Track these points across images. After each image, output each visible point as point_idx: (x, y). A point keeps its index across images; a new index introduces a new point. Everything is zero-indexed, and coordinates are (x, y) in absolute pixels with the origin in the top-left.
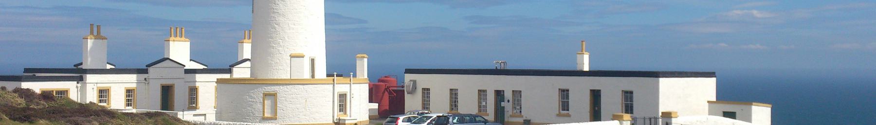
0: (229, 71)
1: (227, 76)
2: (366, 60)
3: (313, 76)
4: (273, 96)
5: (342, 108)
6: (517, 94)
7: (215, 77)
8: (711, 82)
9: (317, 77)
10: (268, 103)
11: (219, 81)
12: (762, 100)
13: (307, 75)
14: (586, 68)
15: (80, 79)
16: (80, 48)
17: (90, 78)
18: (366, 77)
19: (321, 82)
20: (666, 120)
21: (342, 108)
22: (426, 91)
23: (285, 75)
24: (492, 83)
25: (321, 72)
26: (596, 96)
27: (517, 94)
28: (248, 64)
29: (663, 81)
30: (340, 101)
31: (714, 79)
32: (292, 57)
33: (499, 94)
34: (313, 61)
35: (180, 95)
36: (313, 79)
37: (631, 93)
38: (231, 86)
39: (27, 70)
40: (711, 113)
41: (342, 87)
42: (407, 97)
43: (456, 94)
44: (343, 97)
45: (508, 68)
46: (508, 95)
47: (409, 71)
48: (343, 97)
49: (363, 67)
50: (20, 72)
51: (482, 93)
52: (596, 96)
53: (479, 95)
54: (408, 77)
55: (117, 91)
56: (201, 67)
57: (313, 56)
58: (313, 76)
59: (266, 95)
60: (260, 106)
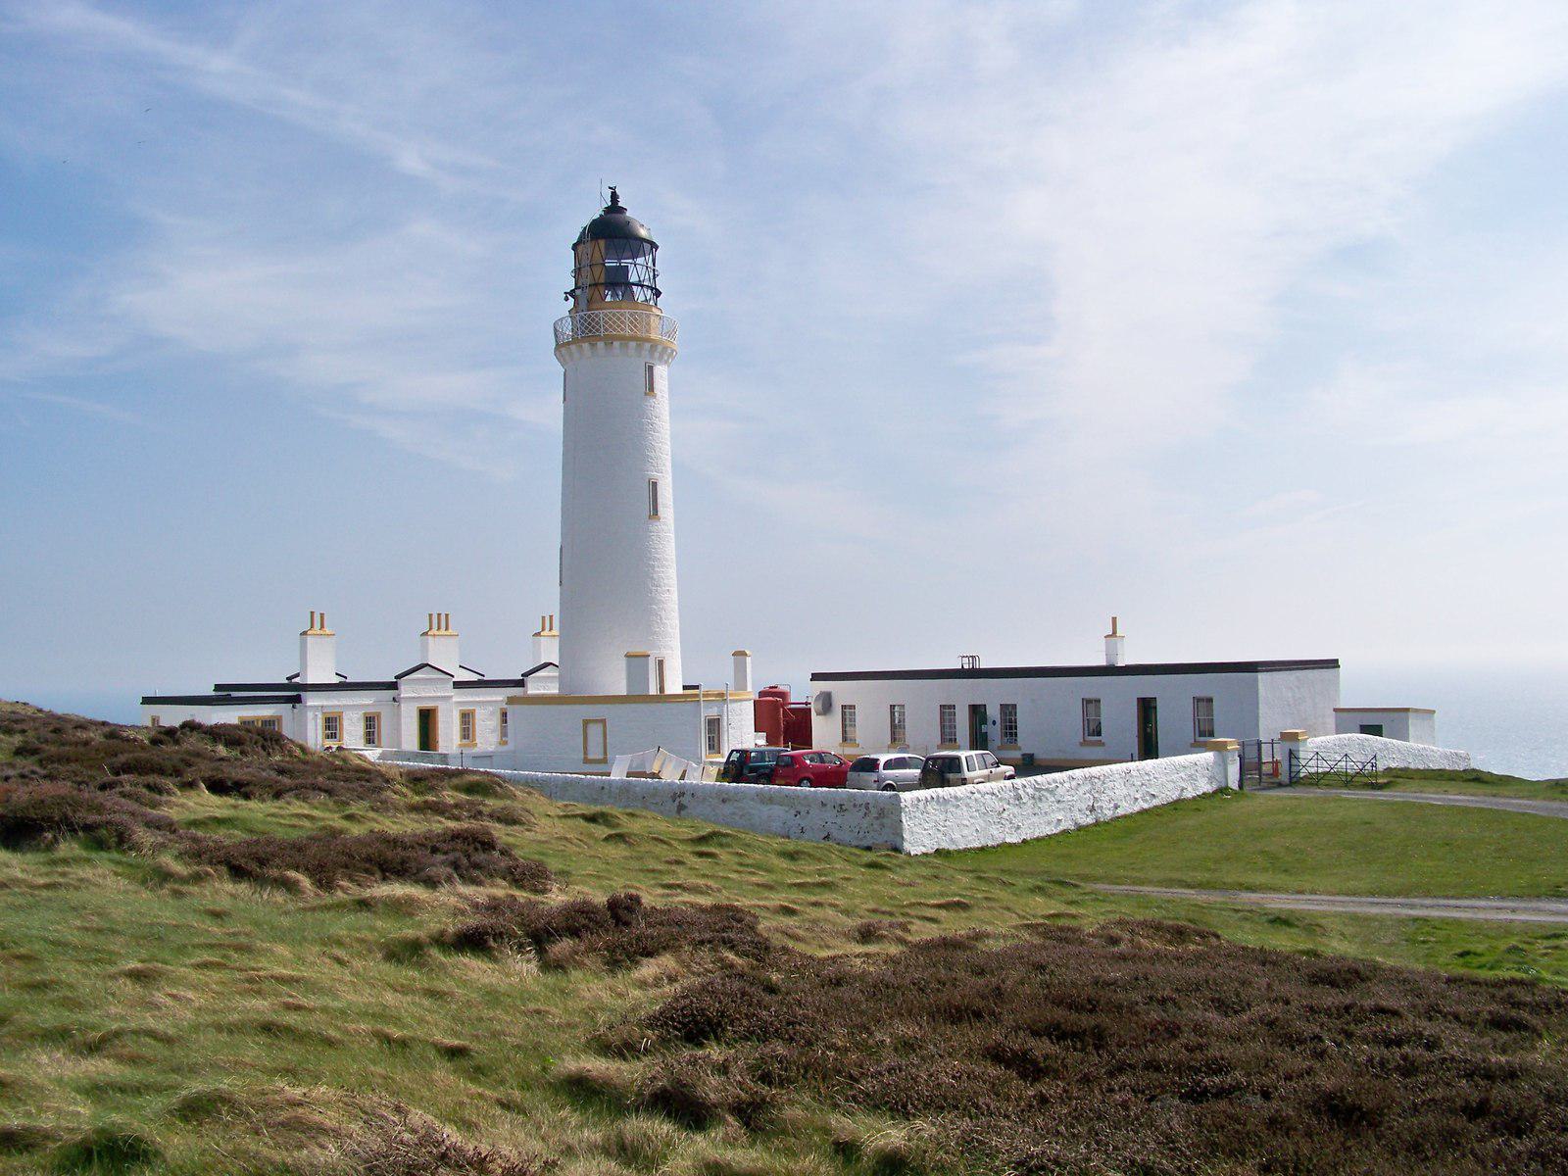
6: (848, 710)
10: (595, 753)
15: (296, 700)
17: (312, 700)
20: (1288, 745)
22: (848, 710)
24: (963, 694)
26: (1204, 703)
27: (1009, 711)
33: (977, 712)
37: (1210, 700)
39: (218, 687)
42: (816, 721)
46: (994, 712)
58: (662, 689)
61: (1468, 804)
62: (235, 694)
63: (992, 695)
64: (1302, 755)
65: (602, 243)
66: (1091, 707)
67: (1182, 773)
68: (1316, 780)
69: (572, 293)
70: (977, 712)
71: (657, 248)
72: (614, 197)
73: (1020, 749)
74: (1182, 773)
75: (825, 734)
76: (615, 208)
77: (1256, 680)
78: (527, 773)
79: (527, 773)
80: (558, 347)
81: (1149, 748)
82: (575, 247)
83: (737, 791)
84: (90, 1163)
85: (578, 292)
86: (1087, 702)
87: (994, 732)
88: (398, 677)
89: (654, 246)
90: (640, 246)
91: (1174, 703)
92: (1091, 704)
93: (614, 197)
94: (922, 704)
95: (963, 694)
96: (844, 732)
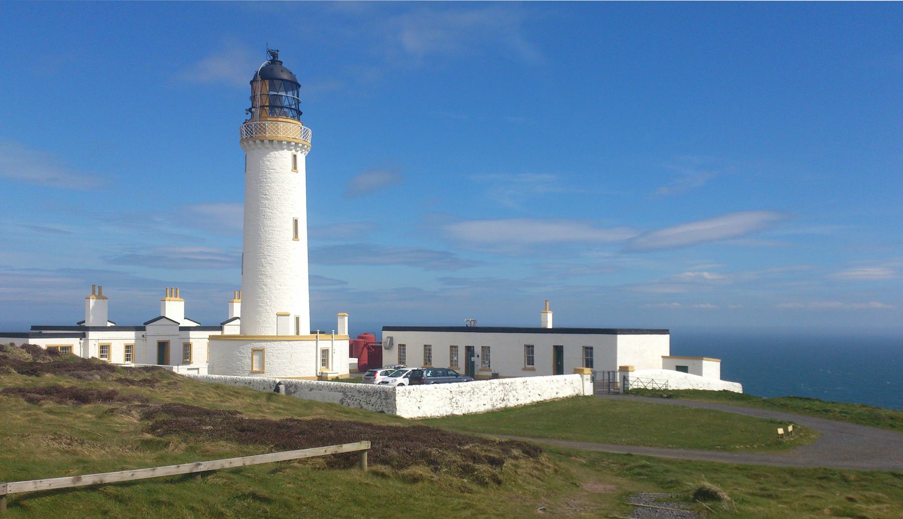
0: (221, 328)
1: (218, 333)
2: (346, 318)
3: (298, 333)
4: (261, 351)
5: (325, 362)
8: (665, 339)
9: (301, 334)
10: (256, 358)
12: (712, 355)
13: (292, 332)
14: (550, 326)
15: (83, 336)
16: (82, 307)
17: (92, 335)
18: (347, 333)
20: (624, 374)
21: (325, 362)
22: (402, 347)
24: (463, 340)
25: (305, 329)
26: (559, 351)
27: (486, 350)
28: (238, 322)
29: (620, 337)
30: (323, 356)
31: (668, 336)
32: (278, 315)
33: (470, 350)
34: (297, 319)
36: (298, 337)
37: (591, 348)
39: (33, 328)
41: (324, 344)
42: (385, 353)
43: (430, 350)
44: (325, 352)
46: (478, 350)
47: (386, 328)
49: (344, 324)
50: (28, 330)
51: (454, 349)
52: (559, 351)
53: (451, 350)
54: (386, 334)
56: (195, 325)
57: (297, 314)
58: (298, 333)
62: (44, 332)
64: (630, 379)
65: (267, 82)
69: (250, 110)
70: (470, 350)
71: (300, 86)
74: (574, 385)
76: (274, 60)
77: (211, 370)
78: (217, 376)
79: (217, 376)
81: (559, 369)
82: (252, 83)
85: (253, 110)
87: (478, 361)
88: (146, 323)
89: (300, 86)
90: (294, 85)
91: (573, 345)
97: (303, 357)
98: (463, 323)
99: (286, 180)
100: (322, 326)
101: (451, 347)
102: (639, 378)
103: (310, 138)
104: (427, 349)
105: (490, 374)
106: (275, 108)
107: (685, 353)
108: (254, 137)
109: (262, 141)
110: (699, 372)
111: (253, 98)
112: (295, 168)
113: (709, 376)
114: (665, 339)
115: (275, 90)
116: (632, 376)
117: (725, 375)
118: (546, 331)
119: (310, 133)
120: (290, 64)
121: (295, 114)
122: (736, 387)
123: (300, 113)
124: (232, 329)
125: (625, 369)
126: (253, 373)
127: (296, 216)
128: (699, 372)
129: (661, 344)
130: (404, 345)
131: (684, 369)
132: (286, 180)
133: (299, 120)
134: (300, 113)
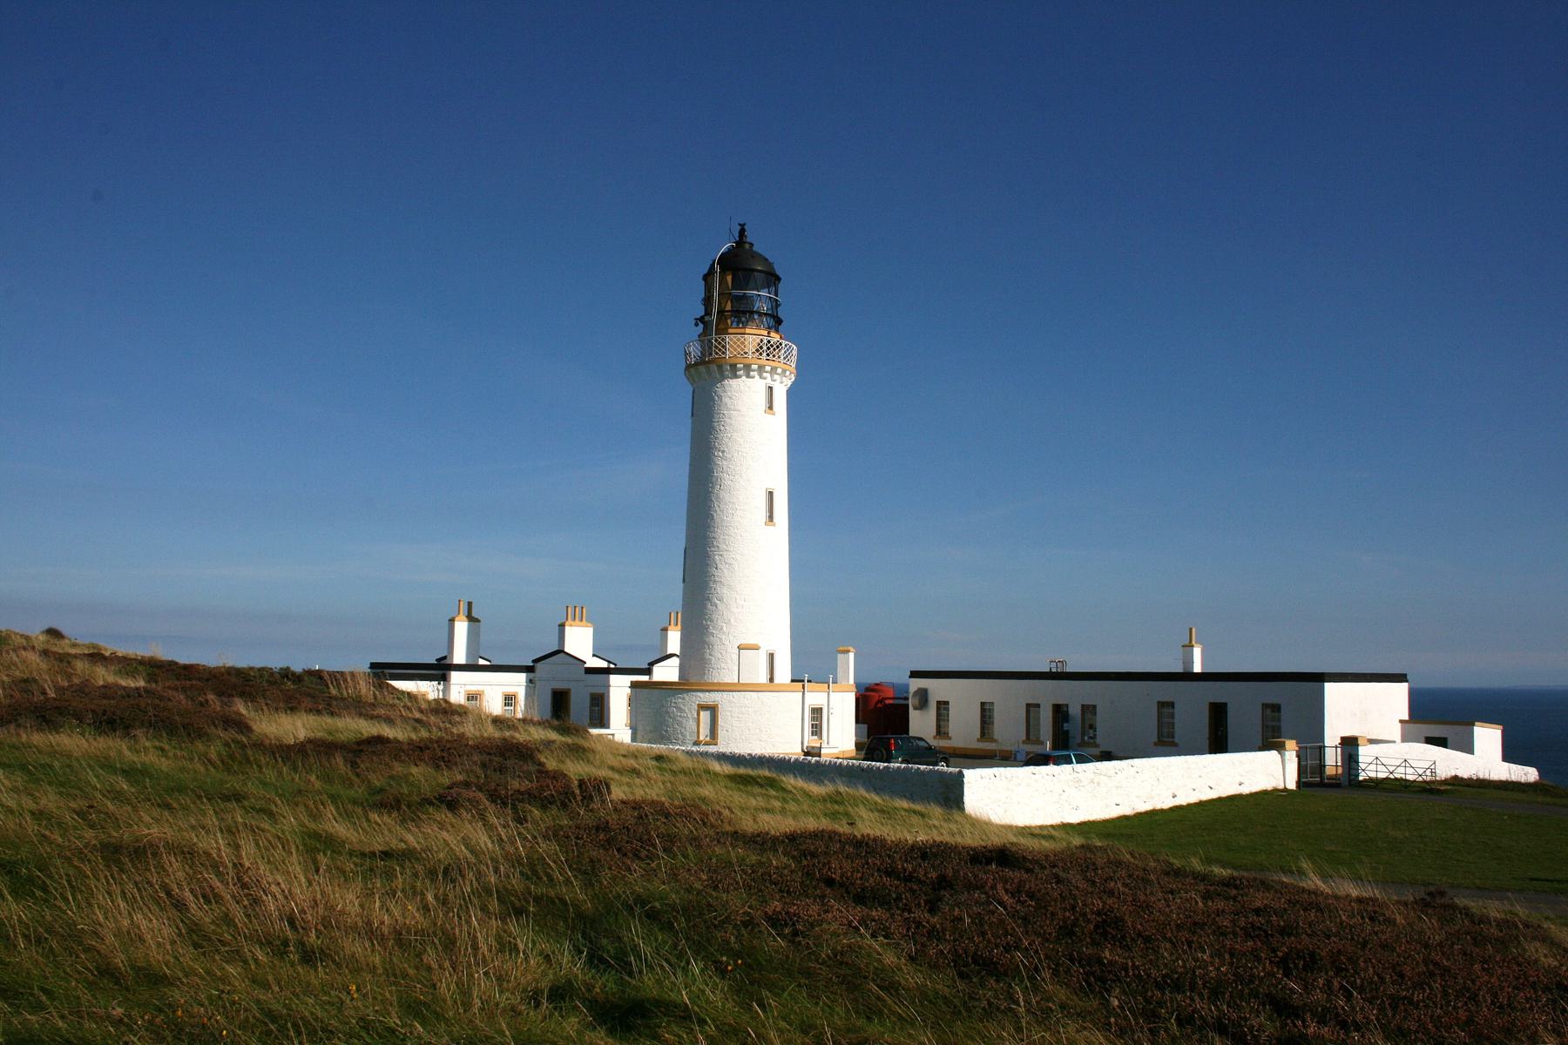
0: (648, 671)
1: (645, 678)
2: (851, 655)
3: (771, 680)
4: (713, 709)
5: (817, 730)
6: (943, 706)
7: (627, 680)
8: (1400, 691)
9: (777, 680)
10: (705, 716)
11: (634, 685)
12: (1489, 719)
13: (763, 678)
14: (1197, 668)
18: (852, 681)
19: (781, 689)
20: (1350, 749)
21: (817, 730)
22: (943, 706)
23: (731, 678)
24: (1047, 694)
25: (784, 673)
26: (1218, 712)
28: (675, 661)
29: (1330, 688)
30: (813, 719)
31: (1405, 685)
33: (1060, 712)
34: (771, 656)
35: (579, 706)
37: (1172, 705)
38: (645, 691)
40: (1405, 739)
41: (816, 698)
42: (914, 715)
43: (991, 711)
44: (817, 712)
45: (1069, 669)
46: (1075, 711)
47: (915, 674)
48: (817, 712)
49: (848, 666)
51: (1031, 708)
52: (1218, 712)
55: (497, 693)
56: (604, 664)
57: (771, 649)
58: (771, 680)
59: (702, 707)
60: (692, 724)
61: (1022, 841)
63: (1074, 696)
66: (1166, 710)
67: (1264, 771)
68: (1376, 784)
69: (701, 319)
72: (742, 232)
73: (1097, 746)
74: (1264, 771)
75: (921, 724)
80: (688, 367)
81: (1218, 745)
83: (870, 769)
84: (584, 750)
86: (1161, 705)
87: (1074, 727)
89: (779, 279)
90: (772, 279)
91: (1244, 705)
92: (1165, 706)
93: (742, 232)
94: (1009, 700)
95: (1047, 694)
96: (938, 726)
97: (778, 710)
98: (1044, 668)
99: (757, 419)
100: (810, 668)
101: (1265, 706)
102: (1371, 764)
103: (794, 359)
104: (986, 712)
105: (1096, 751)
106: (742, 313)
107: (1439, 716)
108: (708, 371)
109: (720, 367)
110: (1467, 747)
111: (707, 301)
112: (771, 517)
113: (1485, 756)
114: (1400, 691)
115: (739, 287)
116: (1365, 753)
117: (1509, 755)
118: (1189, 676)
119: (795, 352)
120: (760, 243)
121: (772, 322)
122: (1529, 774)
123: (779, 322)
124: (667, 672)
125: (1350, 745)
126: (697, 743)
127: (771, 487)
128: (1467, 747)
129: (1393, 700)
130: (947, 703)
131: (1441, 742)
132: (757, 419)
133: (777, 331)
134: (779, 322)
